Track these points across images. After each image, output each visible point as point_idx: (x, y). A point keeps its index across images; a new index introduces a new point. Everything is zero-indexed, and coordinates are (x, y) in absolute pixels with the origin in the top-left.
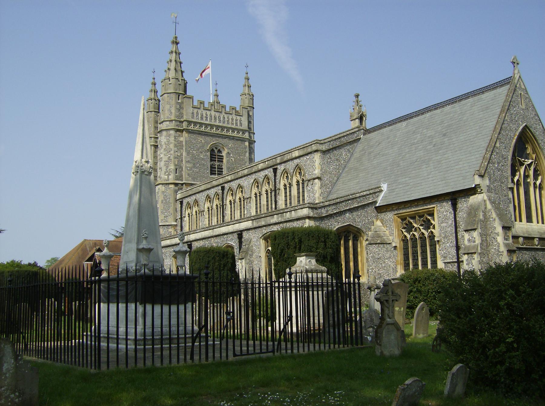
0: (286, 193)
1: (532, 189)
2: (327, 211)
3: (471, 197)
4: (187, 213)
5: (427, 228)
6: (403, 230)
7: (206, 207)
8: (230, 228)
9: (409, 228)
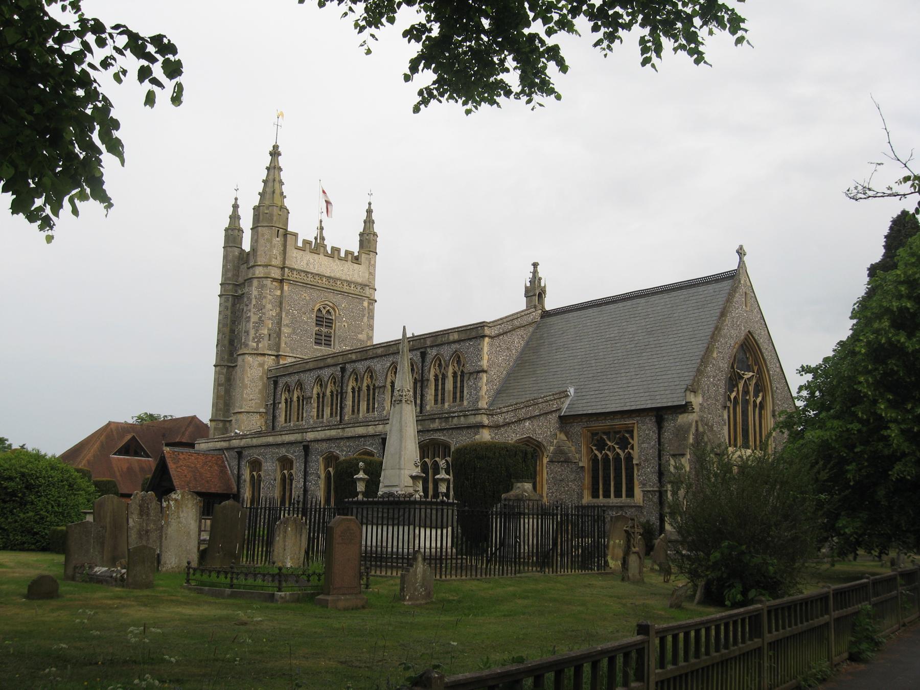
1: (750, 408)
2: (505, 419)
3: (680, 416)
4: (283, 398)
5: (623, 448)
6: (594, 448)
7: (315, 392)
9: (601, 446)
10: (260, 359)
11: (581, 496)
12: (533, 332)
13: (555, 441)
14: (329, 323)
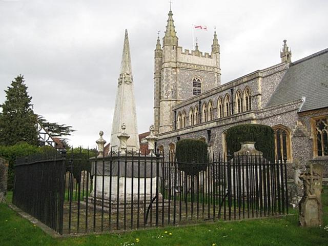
0: (239, 105)
6: (317, 128)
7: (190, 114)
8: (203, 127)
10: (169, 102)
11: (312, 155)
12: (286, 74)
13: (296, 126)
14: (200, 85)
